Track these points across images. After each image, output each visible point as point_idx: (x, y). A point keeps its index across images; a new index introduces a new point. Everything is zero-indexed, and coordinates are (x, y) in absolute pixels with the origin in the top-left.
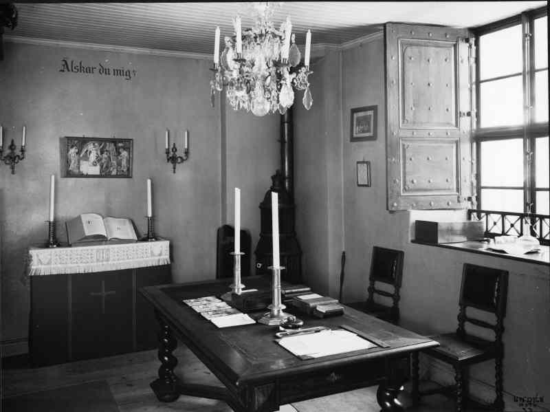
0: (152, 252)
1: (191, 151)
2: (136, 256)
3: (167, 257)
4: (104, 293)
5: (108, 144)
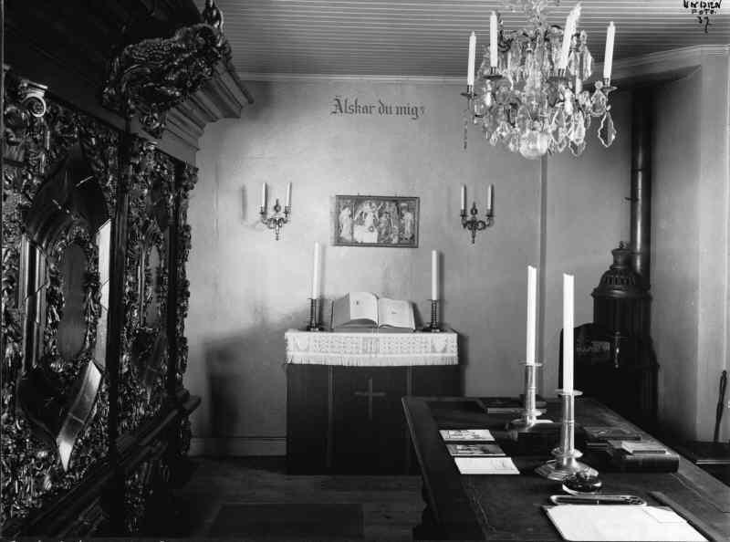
0: (433, 347)
1: (496, 212)
2: (423, 350)
3: (455, 354)
4: (371, 394)
5: (387, 203)
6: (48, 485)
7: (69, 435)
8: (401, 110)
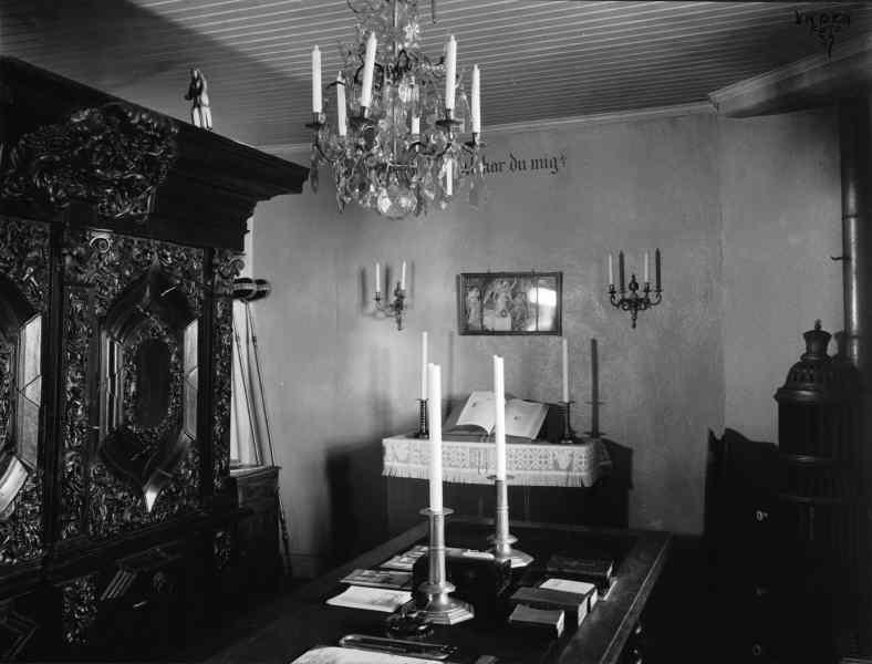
6: (128, 516)
7: (156, 484)
8: (535, 164)
